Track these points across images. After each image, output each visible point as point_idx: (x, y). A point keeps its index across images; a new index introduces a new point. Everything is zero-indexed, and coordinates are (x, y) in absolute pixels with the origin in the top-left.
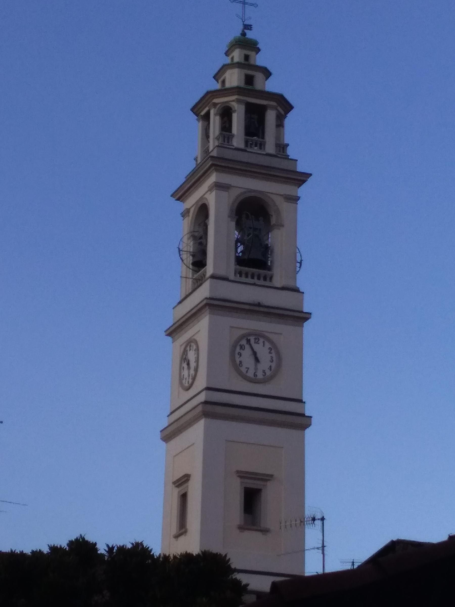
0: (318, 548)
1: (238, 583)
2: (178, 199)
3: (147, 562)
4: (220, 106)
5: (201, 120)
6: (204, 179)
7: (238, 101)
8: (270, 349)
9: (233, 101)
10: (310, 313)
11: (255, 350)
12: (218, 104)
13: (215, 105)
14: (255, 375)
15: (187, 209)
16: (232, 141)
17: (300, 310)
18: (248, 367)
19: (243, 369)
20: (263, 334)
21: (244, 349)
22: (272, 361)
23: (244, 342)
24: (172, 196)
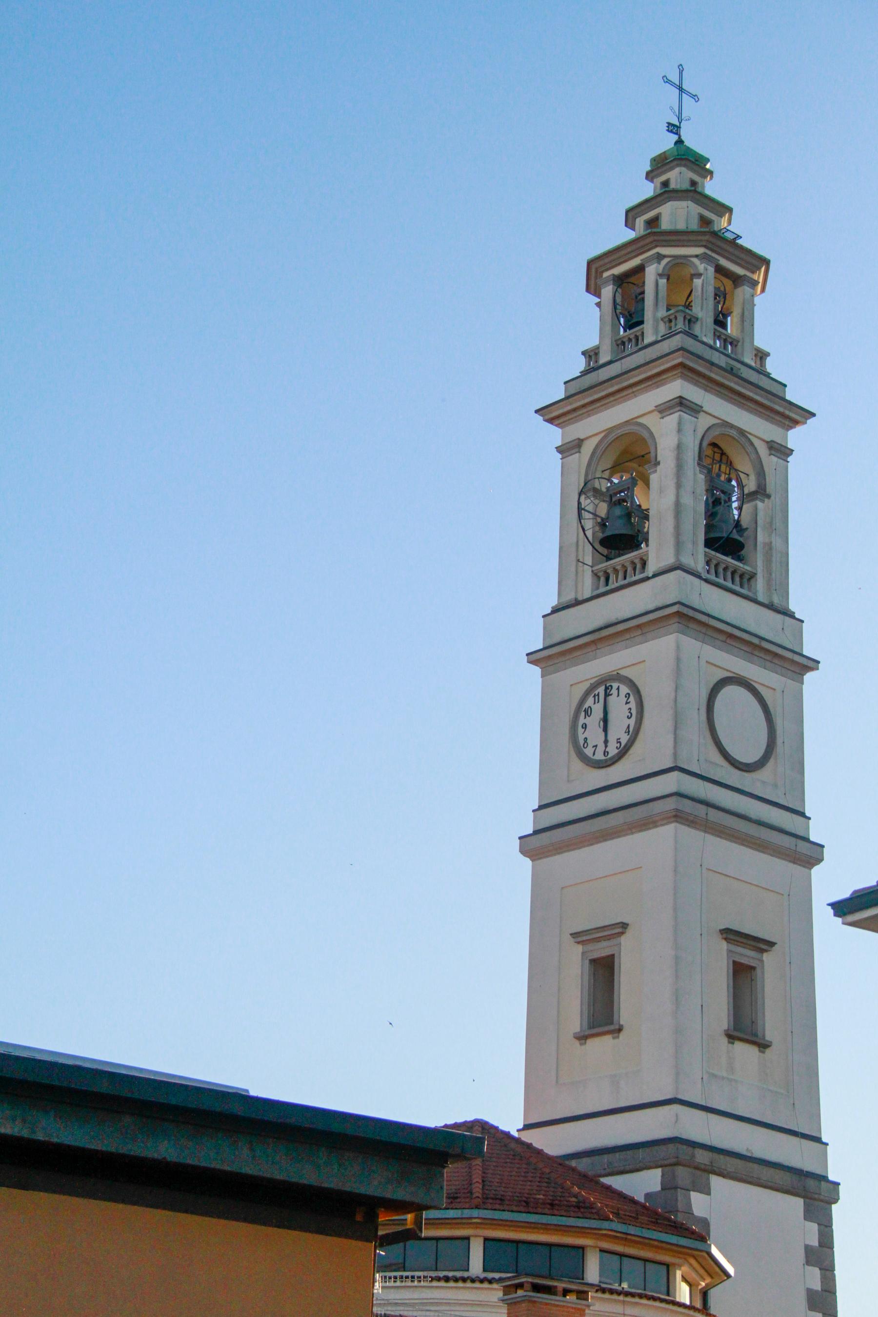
0: (645, 1263)
1: (759, 269)
2: (550, 421)
3: (715, 492)
4: (669, 262)
5: (612, 282)
6: (598, 407)
7: (703, 257)
8: (627, 695)
9: (697, 256)
10: (556, 449)
11: (603, 734)
12: (665, 256)
13: (660, 257)
14: (605, 753)
15: (579, 439)
16: (568, 1283)
17: (805, 836)
18: (595, 744)
19: (589, 751)
20: (676, 180)
21: (587, 747)
22: (629, 716)
23: (601, 690)
24: (556, 448)
